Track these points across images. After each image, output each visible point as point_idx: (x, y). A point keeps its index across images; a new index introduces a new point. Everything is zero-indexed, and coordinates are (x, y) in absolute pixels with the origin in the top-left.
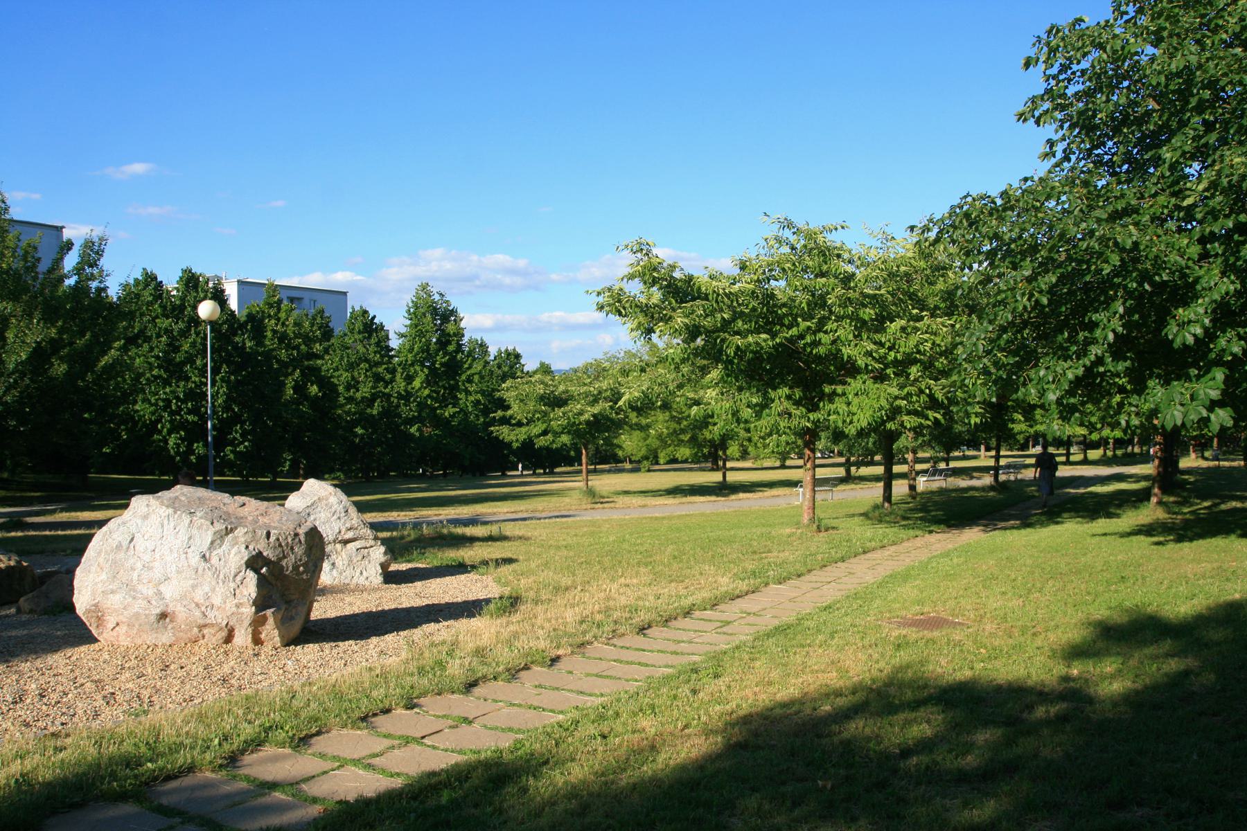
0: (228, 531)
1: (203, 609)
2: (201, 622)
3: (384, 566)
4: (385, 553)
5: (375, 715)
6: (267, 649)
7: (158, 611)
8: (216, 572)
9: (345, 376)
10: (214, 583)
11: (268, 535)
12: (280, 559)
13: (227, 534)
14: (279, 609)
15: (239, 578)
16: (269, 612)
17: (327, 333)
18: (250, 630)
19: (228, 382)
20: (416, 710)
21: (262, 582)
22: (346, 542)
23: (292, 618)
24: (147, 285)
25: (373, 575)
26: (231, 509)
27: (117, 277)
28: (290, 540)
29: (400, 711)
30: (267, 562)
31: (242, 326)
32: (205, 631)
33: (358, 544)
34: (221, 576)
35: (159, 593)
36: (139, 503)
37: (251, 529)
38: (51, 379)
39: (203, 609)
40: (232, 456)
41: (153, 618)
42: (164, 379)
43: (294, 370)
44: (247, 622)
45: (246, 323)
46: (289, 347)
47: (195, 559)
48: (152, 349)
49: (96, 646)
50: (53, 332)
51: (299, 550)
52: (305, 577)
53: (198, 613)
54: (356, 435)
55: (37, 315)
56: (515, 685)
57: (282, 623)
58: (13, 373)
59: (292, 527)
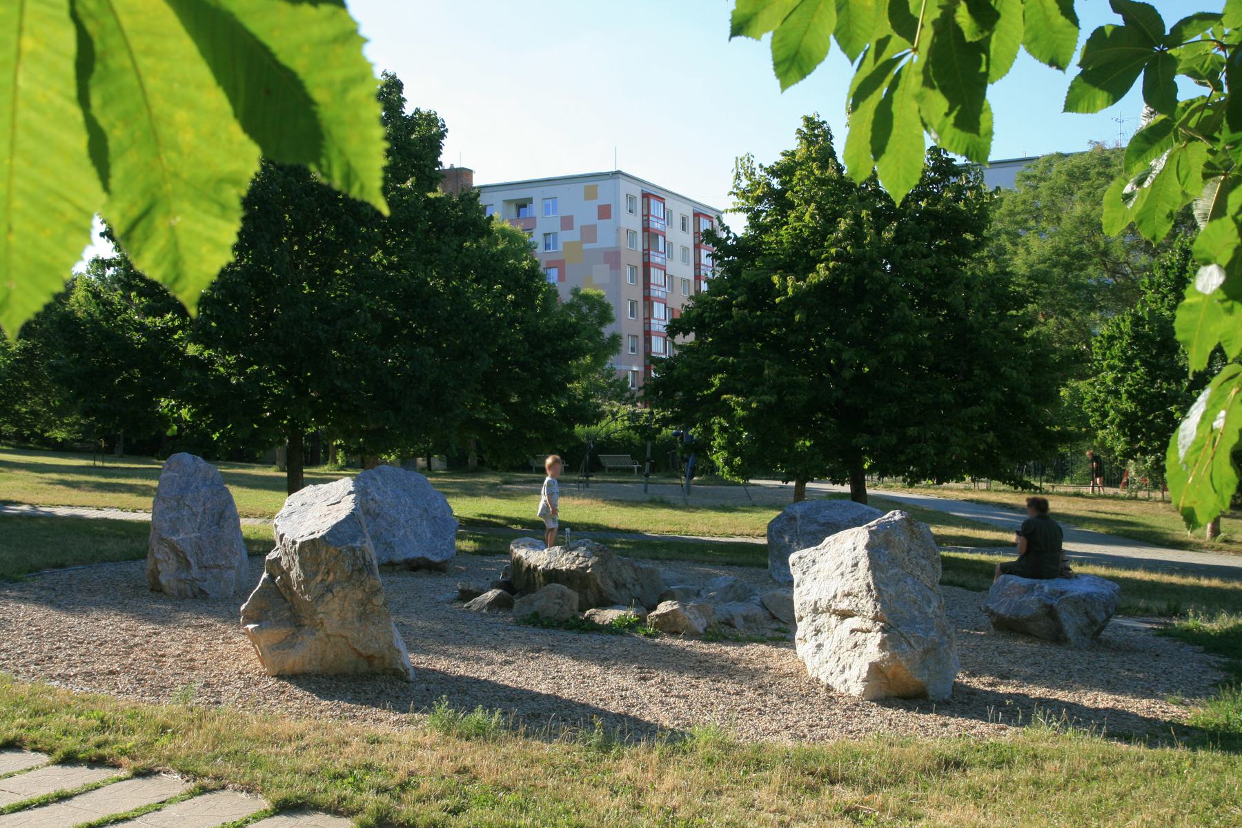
22: (844, 615)
23: (292, 646)
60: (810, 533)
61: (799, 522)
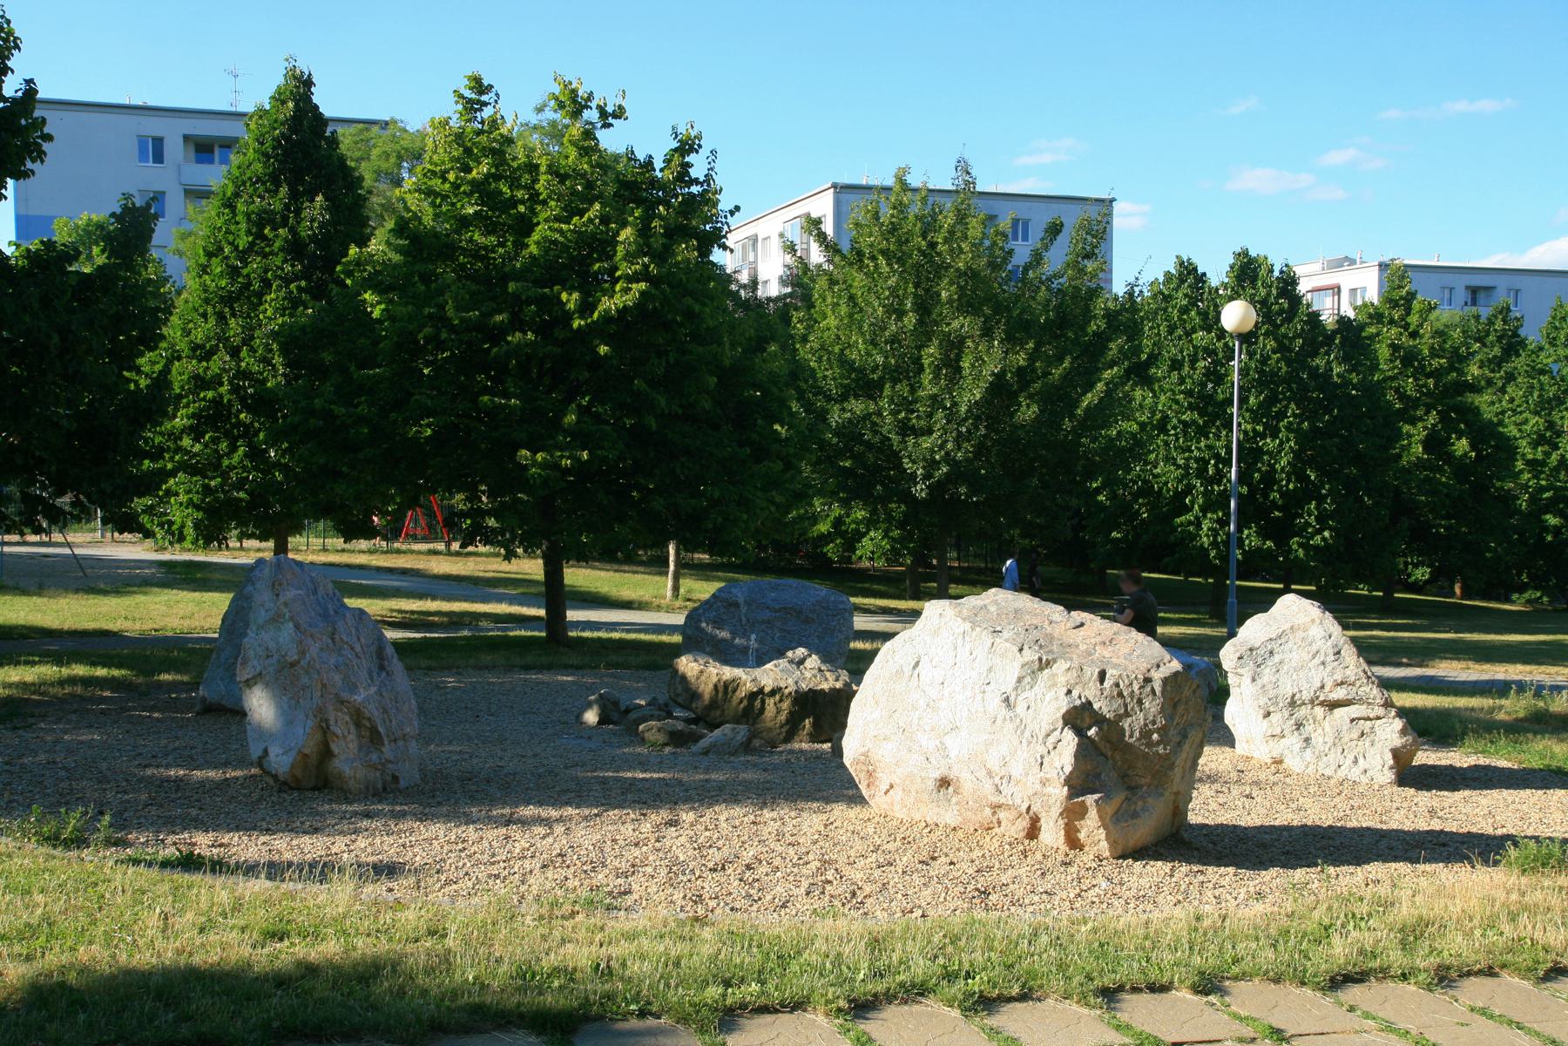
0: (1044, 665)
1: (997, 780)
2: (995, 799)
3: (1401, 759)
4: (1403, 732)
5: (1135, 990)
6: (1087, 858)
7: (937, 775)
8: (1021, 727)
9: (1535, 422)
10: (1016, 742)
11: (1102, 676)
12: (1120, 717)
13: (1041, 669)
14: (1107, 797)
15: (1051, 740)
16: (1090, 800)
17: (1513, 344)
18: (1061, 822)
19: (1298, 432)
20: (1212, 998)
21: (1085, 750)
22: (1333, 705)
23: (1135, 815)
24: (1182, 281)
25: (1379, 766)
26: (1057, 631)
27: (1135, 265)
28: (1136, 687)
29: (1185, 994)
30: (1099, 719)
31: (1329, 339)
32: (1002, 815)
33: (1354, 711)
34: (1027, 734)
35: (942, 749)
36: (935, 611)
37: (1076, 664)
38: (1016, 427)
39: (997, 780)
40: (1301, 553)
41: (931, 785)
42: (1198, 426)
43: (1427, 413)
44: (1056, 810)
45: (1335, 332)
46: (1420, 372)
47: (995, 703)
48: (1182, 381)
49: (864, 813)
50: (1021, 359)
51: (1152, 706)
52: (1161, 750)
53: (988, 787)
54: (1546, 528)
55: (999, 333)
56: (1440, 996)
57: (1114, 822)
58: (965, 420)
59: (1144, 666)
60: (763, 622)
61: (744, 609)
